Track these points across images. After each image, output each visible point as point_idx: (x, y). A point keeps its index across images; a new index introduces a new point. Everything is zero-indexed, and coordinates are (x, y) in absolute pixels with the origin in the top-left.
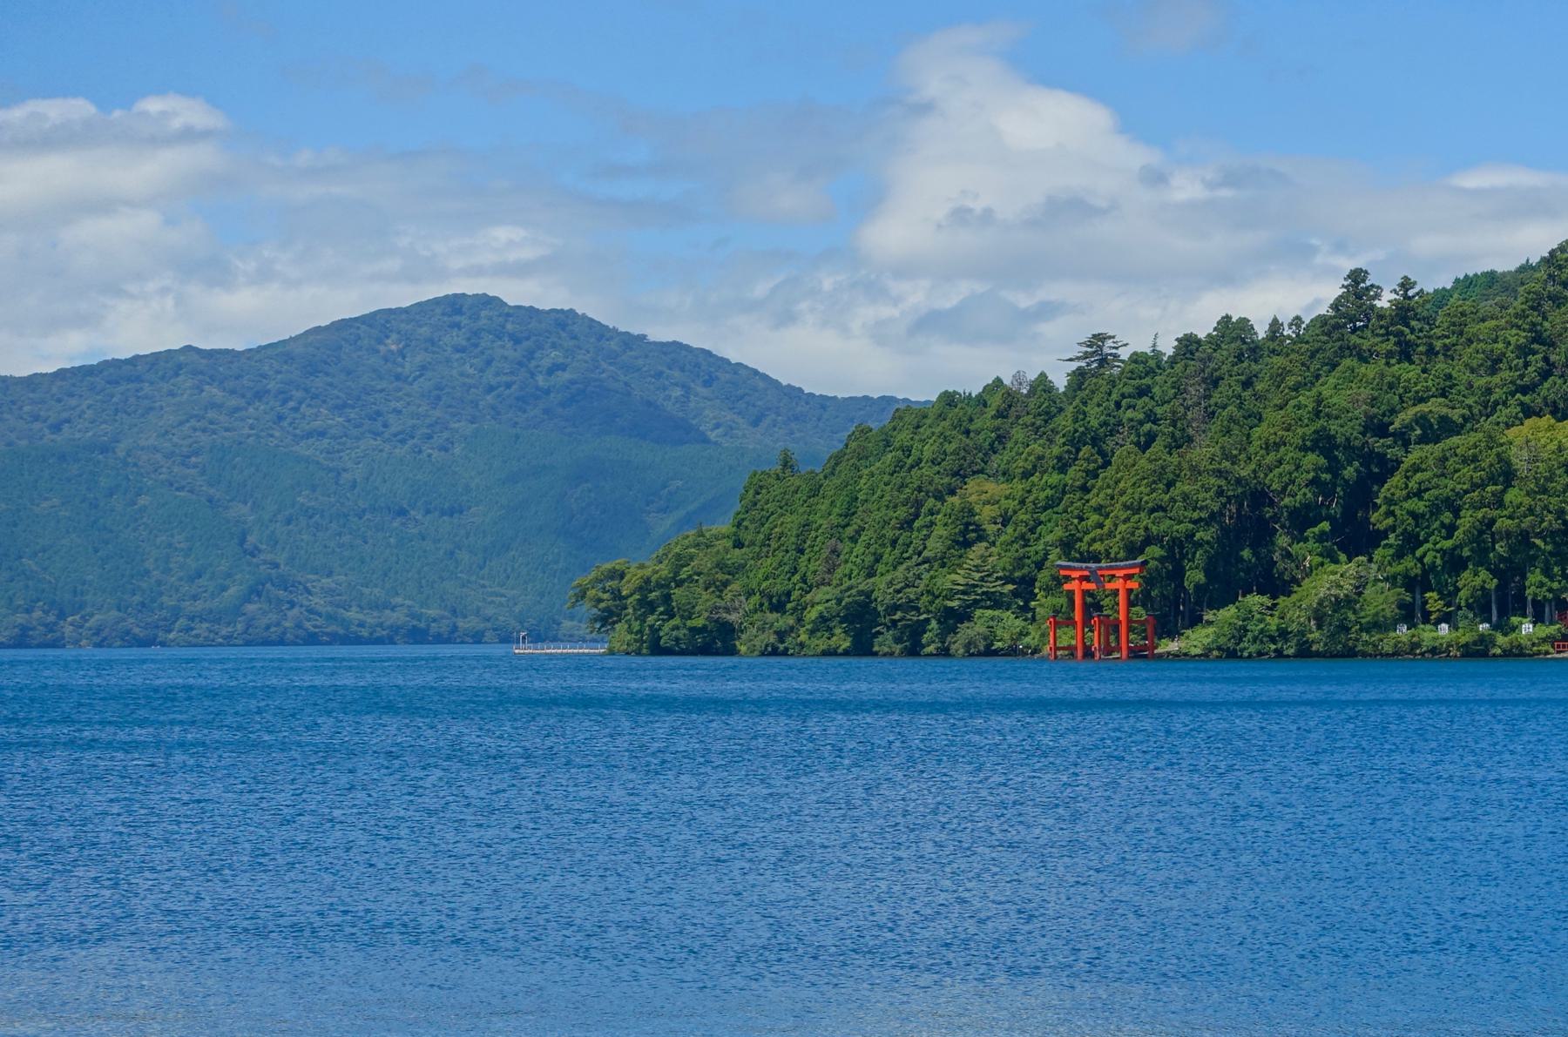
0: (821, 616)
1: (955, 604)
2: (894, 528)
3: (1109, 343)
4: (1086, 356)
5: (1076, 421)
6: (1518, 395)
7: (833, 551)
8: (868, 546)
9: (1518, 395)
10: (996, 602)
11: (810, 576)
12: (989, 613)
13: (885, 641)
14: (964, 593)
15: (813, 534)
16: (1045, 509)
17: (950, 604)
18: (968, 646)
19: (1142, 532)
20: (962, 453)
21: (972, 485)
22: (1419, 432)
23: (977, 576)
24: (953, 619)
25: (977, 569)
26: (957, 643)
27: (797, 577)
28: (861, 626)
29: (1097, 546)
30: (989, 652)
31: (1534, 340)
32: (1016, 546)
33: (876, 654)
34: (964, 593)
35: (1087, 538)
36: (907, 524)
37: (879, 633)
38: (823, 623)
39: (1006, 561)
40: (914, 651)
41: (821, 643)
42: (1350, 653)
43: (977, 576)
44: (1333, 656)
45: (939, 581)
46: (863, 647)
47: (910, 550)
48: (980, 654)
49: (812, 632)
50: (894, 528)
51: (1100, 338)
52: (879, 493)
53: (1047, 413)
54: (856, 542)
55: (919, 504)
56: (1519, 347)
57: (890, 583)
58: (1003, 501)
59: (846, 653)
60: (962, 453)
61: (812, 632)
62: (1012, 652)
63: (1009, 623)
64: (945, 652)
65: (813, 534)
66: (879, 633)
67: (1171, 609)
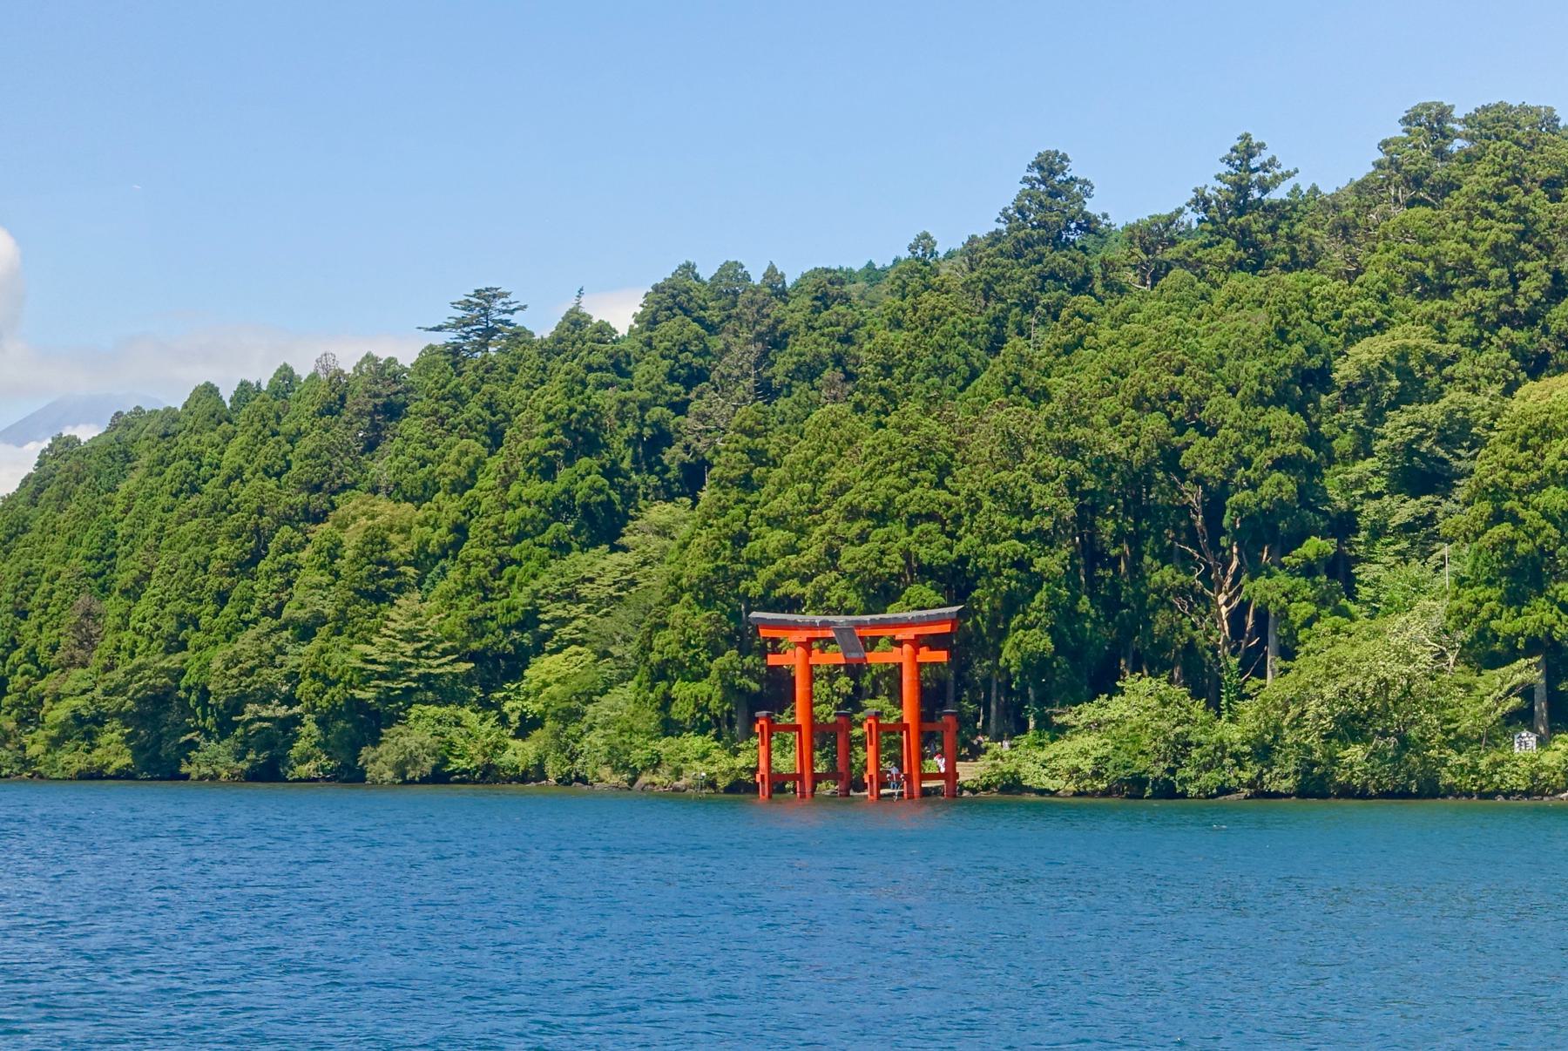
0: (77, 717)
1: (368, 695)
2: (221, 573)
3: (498, 304)
4: (461, 323)
5: (570, 394)
6: (1505, 330)
7: (87, 614)
8: (162, 604)
9: (1505, 330)
10: (448, 693)
11: (42, 652)
12: (433, 710)
13: (216, 755)
14: (382, 676)
15: (45, 586)
16: (517, 538)
17: (359, 694)
18: (400, 769)
19: (897, 557)
20: (326, 456)
21: (348, 504)
22: (1395, 383)
23: (409, 648)
24: (364, 723)
25: (411, 636)
26: (380, 760)
27: (17, 655)
28: (159, 739)
29: (792, 587)
30: (439, 777)
31: (1522, 236)
32: (466, 601)
33: (287, 781)
34: (382, 676)
35: (764, 574)
36: (246, 565)
37: (192, 745)
38: (85, 727)
39: (454, 622)
40: (269, 772)
41: (73, 759)
42: (1431, 790)
43: (409, 648)
44: (1405, 794)
45: (337, 657)
46: (158, 763)
47: (255, 610)
48: (424, 780)
49: (56, 743)
50: (221, 573)
51: (487, 296)
52: (155, 524)
53: (456, 396)
54: (137, 598)
55: (261, 539)
56: (1496, 248)
57: (234, 661)
58: (416, 529)
59: (123, 775)
60: (326, 456)
61: (56, 743)
62: (489, 774)
63: (474, 732)
64: (350, 774)
65: (45, 586)
66: (192, 745)
67: (969, 696)
